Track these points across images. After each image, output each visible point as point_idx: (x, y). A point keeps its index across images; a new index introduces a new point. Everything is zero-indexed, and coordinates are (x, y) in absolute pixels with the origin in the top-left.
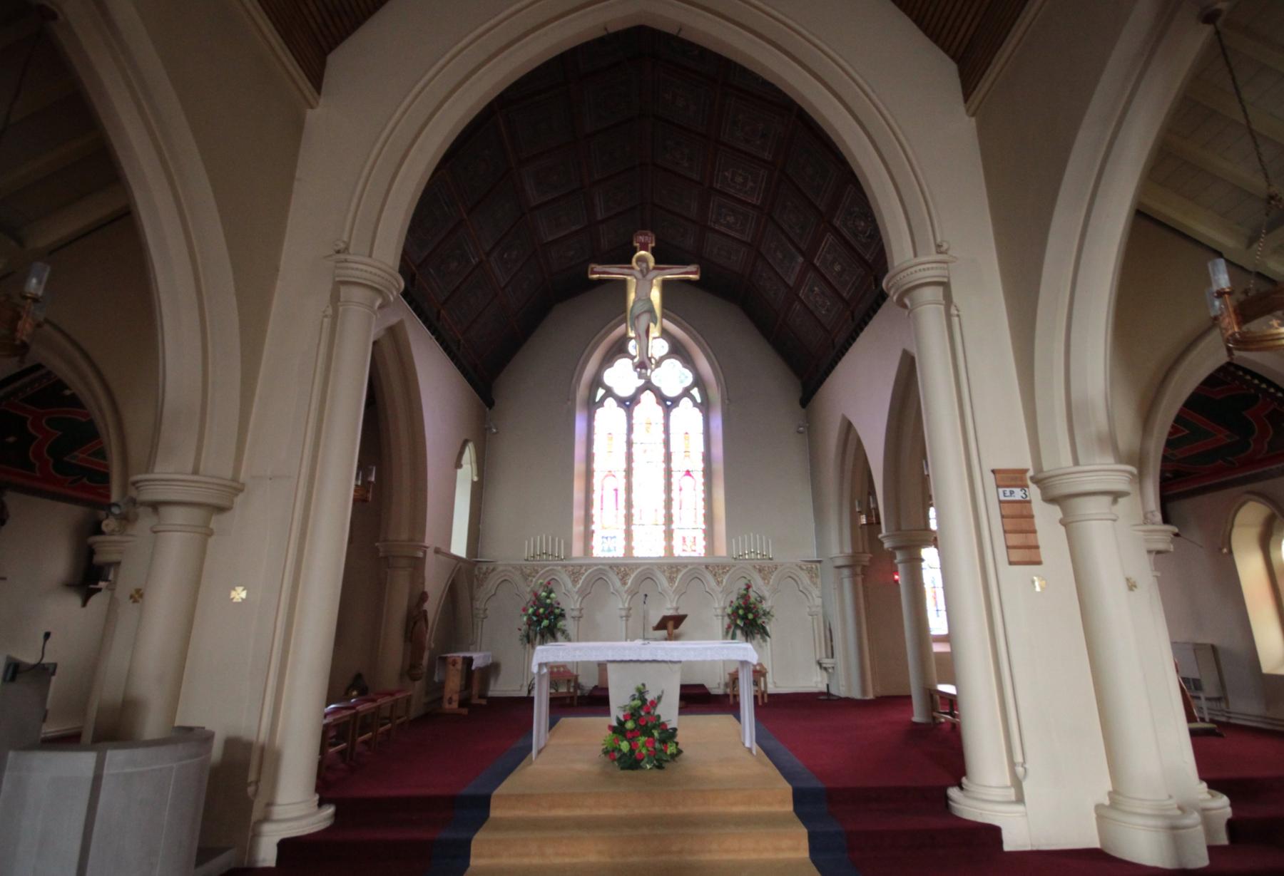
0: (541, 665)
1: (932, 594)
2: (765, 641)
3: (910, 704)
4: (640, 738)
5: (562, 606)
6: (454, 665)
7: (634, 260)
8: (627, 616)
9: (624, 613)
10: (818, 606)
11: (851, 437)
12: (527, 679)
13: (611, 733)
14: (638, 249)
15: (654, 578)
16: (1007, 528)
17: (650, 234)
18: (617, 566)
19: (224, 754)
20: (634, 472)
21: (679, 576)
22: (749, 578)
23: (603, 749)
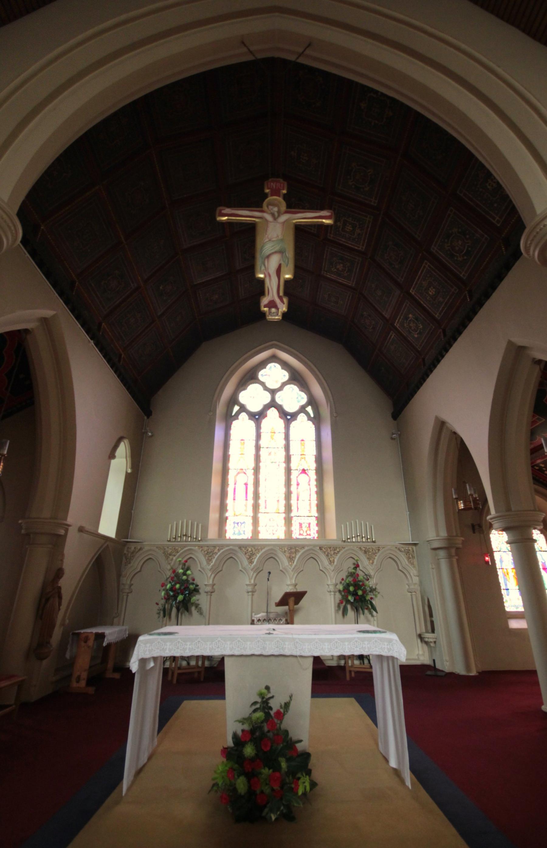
4: (263, 771)
5: (197, 581)
7: (265, 204)
8: (253, 592)
9: (250, 588)
10: (416, 584)
14: (269, 195)
15: (276, 558)
17: (281, 180)
18: (246, 547)
20: (261, 470)
21: (297, 557)
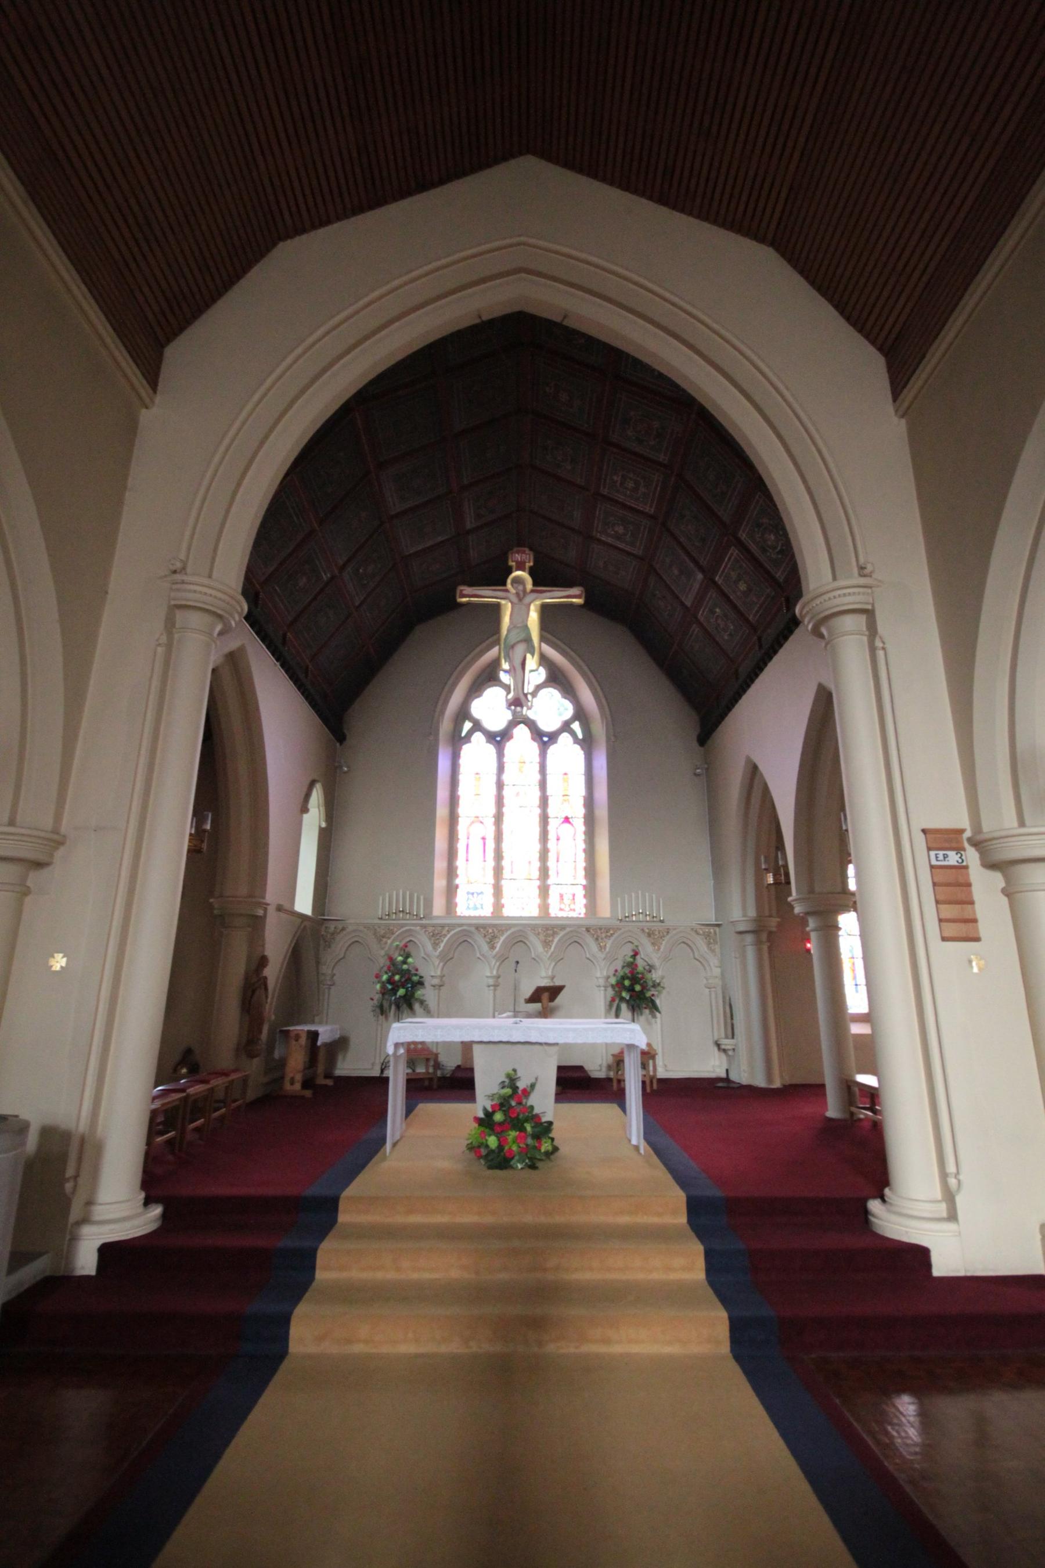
0: (397, 1045)
1: (850, 965)
2: (654, 1017)
3: (824, 1095)
4: (510, 1132)
5: (421, 972)
6: (297, 1040)
7: (509, 581)
9: (491, 982)
11: (756, 781)
12: (380, 1057)
13: (476, 1125)
14: (514, 569)
15: (527, 942)
16: (941, 898)
17: (527, 550)
19: (40, 1146)
21: (556, 940)
22: (636, 943)
23: (468, 1144)
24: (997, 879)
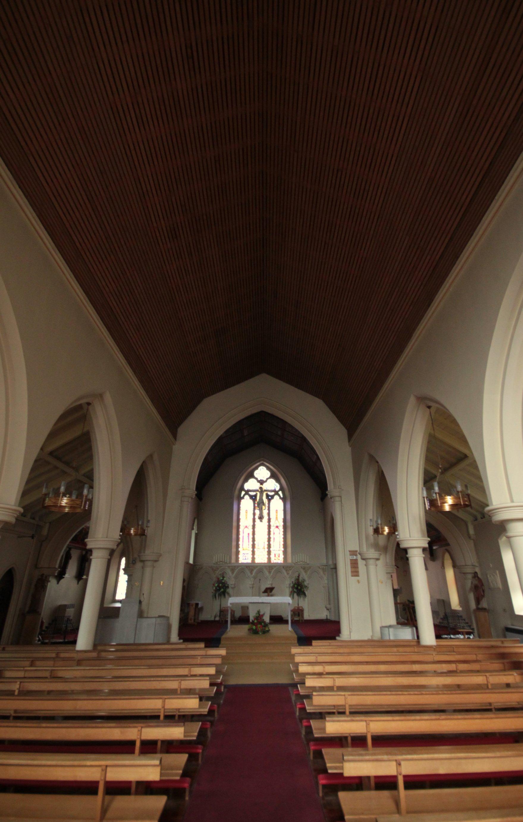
5: (228, 583)
8: (253, 587)
9: (251, 586)
24: (364, 562)
